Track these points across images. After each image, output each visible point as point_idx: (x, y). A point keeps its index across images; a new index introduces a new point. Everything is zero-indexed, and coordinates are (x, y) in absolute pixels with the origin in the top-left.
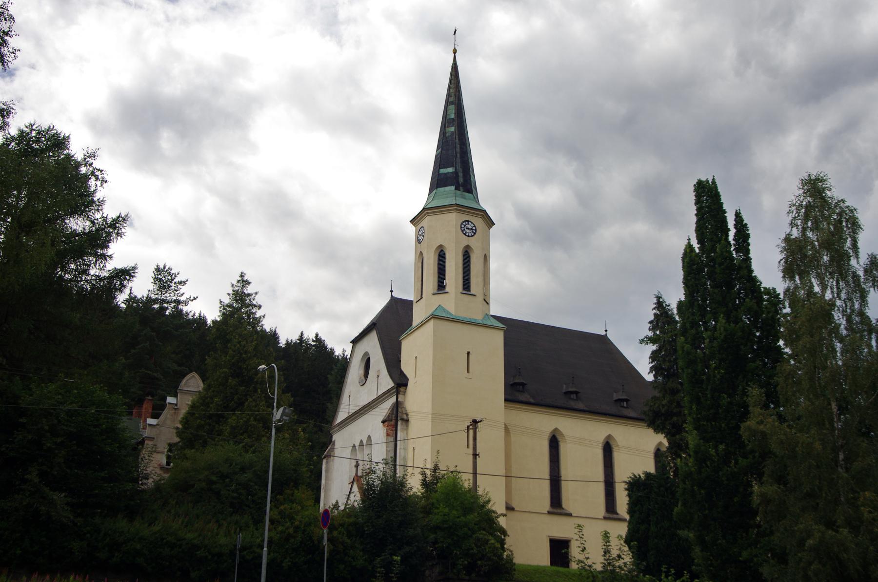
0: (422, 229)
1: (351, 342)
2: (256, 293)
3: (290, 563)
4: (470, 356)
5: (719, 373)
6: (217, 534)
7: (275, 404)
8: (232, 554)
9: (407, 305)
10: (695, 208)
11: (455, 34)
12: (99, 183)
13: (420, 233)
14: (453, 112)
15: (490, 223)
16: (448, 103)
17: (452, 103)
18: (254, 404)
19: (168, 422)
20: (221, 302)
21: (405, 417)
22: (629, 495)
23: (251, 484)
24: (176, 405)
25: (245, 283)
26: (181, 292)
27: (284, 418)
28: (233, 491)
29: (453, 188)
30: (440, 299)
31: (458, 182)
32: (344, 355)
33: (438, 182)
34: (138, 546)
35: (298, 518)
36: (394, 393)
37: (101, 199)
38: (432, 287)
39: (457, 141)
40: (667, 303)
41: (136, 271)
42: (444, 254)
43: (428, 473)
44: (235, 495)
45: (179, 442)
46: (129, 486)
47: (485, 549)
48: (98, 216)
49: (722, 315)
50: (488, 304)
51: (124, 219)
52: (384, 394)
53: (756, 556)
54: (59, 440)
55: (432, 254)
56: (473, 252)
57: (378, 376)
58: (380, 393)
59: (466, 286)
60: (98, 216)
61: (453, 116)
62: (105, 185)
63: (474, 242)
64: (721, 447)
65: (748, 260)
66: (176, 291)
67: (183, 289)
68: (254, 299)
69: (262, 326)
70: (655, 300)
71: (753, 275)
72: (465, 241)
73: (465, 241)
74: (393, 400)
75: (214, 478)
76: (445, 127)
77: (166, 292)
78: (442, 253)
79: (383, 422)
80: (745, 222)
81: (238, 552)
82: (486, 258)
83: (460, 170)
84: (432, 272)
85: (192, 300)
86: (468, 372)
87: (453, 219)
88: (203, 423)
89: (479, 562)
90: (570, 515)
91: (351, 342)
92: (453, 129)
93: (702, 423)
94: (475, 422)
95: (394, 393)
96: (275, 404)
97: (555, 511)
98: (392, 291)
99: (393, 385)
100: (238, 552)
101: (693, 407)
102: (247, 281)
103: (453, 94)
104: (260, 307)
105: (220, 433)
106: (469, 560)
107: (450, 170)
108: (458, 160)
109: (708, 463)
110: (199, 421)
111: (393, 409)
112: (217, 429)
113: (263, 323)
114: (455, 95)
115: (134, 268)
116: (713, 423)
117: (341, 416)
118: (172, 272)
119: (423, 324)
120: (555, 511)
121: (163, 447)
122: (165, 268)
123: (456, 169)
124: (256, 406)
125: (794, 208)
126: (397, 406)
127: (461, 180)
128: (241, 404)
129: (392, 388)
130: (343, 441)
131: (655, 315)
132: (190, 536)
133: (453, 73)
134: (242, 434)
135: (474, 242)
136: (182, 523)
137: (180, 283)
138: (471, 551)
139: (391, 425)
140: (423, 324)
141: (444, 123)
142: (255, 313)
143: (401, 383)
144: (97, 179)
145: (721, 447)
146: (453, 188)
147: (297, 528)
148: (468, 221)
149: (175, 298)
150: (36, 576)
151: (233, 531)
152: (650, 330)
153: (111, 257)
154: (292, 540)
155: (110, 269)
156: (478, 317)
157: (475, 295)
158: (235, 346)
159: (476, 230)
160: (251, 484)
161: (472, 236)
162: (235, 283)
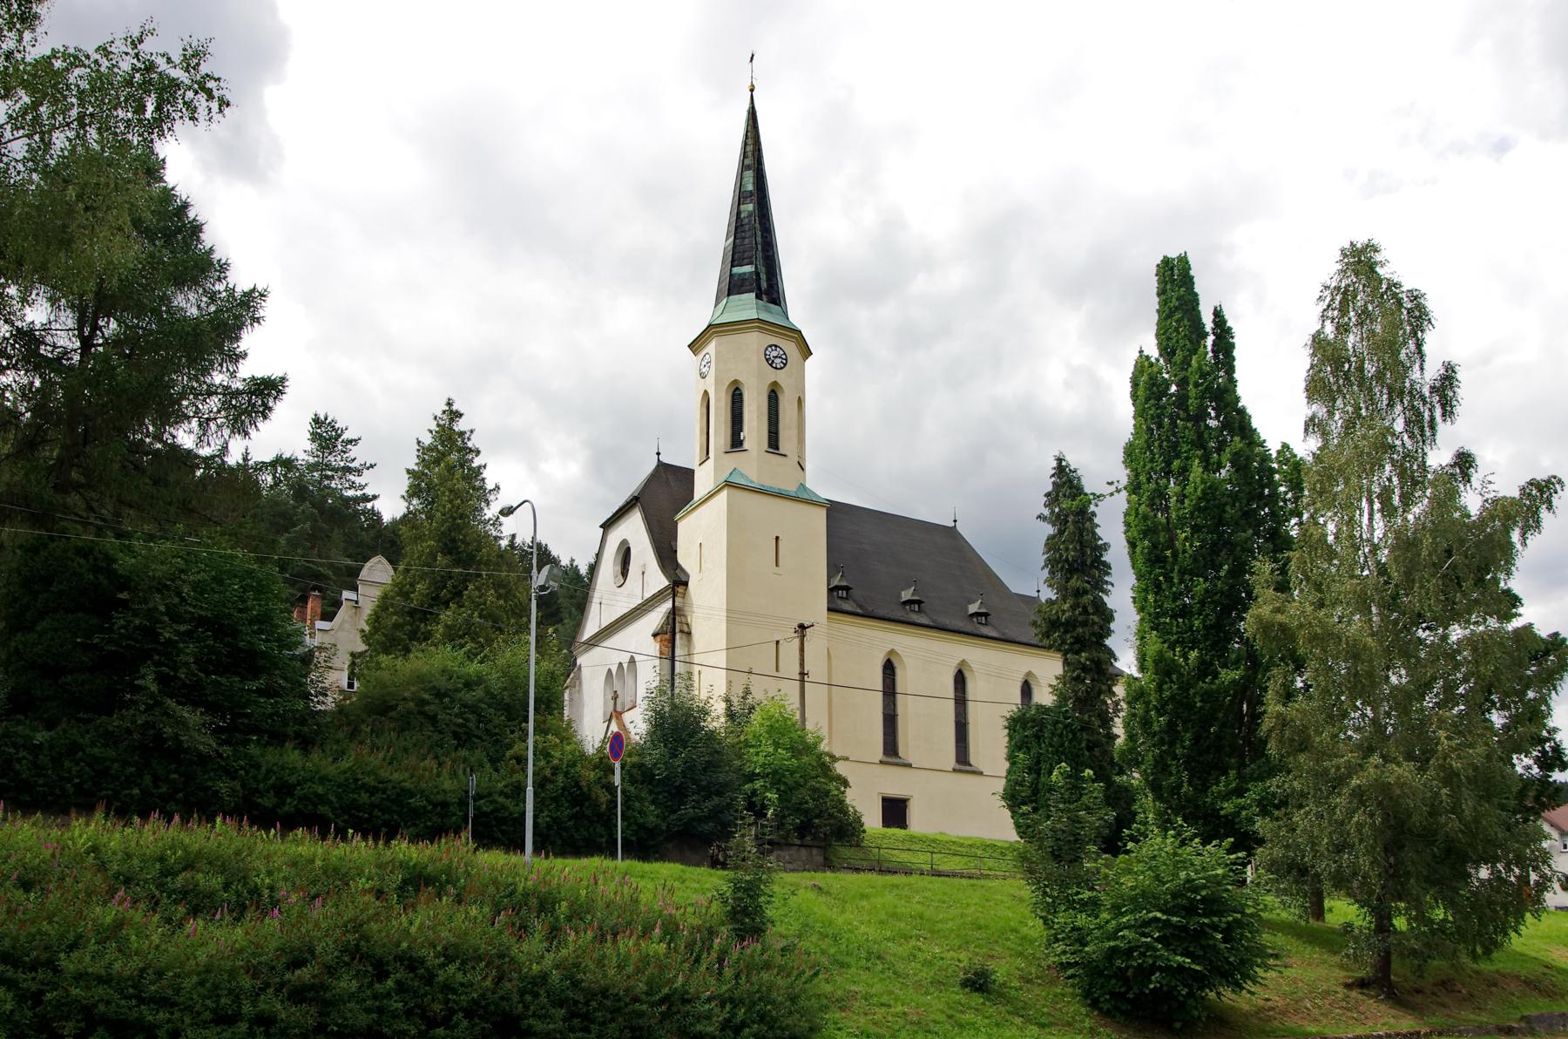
0: (707, 356)
1: (601, 526)
2: (472, 431)
3: (548, 819)
4: (780, 542)
5: (1191, 546)
6: (438, 775)
7: (534, 562)
8: (463, 803)
9: (686, 476)
10: (1157, 299)
11: (751, 60)
12: (215, 105)
13: (704, 363)
14: (751, 180)
15: (806, 352)
16: (743, 167)
17: (748, 168)
18: (477, 593)
19: (347, 626)
20: (419, 442)
21: (686, 629)
22: (1009, 735)
23: (483, 706)
24: (357, 602)
25: (455, 415)
26: (352, 455)
27: (551, 583)
28: (456, 715)
29: (753, 295)
30: (735, 459)
31: (759, 288)
32: (572, 565)
33: (733, 286)
34: (320, 790)
35: (557, 754)
36: (668, 594)
37: (223, 261)
38: (723, 442)
39: (757, 225)
40: (1072, 468)
41: (287, 384)
42: (741, 395)
43: (735, 701)
44: (461, 721)
45: (366, 651)
46: (300, 705)
47: (826, 803)
48: (220, 287)
49: (1197, 461)
50: (803, 469)
51: (262, 295)
52: (654, 597)
53: (1243, 808)
54: (183, 628)
55: (723, 394)
56: (783, 392)
57: (643, 573)
58: (648, 595)
59: (774, 443)
60: (220, 287)
61: (750, 187)
62: (227, 111)
63: (781, 377)
64: (1194, 654)
65: (1232, 382)
66: (345, 452)
67: (354, 451)
68: (469, 439)
69: (483, 479)
70: (1054, 464)
71: (1240, 405)
72: (772, 375)
73: (772, 375)
74: (668, 605)
75: (426, 696)
76: (739, 204)
77: (330, 454)
78: (738, 392)
79: (655, 635)
80: (1228, 324)
81: (471, 801)
82: (800, 402)
83: (762, 270)
84: (723, 419)
85: (368, 469)
86: (777, 565)
87: (755, 342)
88: (401, 621)
89: (817, 821)
90: (910, 766)
91: (601, 526)
92: (750, 207)
93: (1162, 620)
94: (802, 627)
95: (668, 594)
96: (534, 562)
97: (889, 760)
98: (658, 454)
99: (667, 583)
100: (471, 801)
101: (1149, 597)
102: (457, 411)
103: (750, 154)
104: (478, 452)
105: (427, 636)
106: (802, 818)
107: (748, 269)
108: (760, 254)
109: (1174, 677)
110: (395, 617)
111: (668, 617)
112: (423, 630)
113: (483, 476)
114: (753, 155)
115: (283, 379)
116: (1180, 620)
117: (590, 628)
118: (337, 426)
119: (711, 496)
120: (889, 760)
121: (342, 661)
122: (326, 419)
123: (756, 268)
124: (480, 597)
125: (1327, 293)
126: (674, 613)
127: (764, 285)
128: (457, 594)
129: (666, 589)
130: (593, 666)
131: (1054, 483)
132: (396, 776)
133: (751, 122)
134: (461, 637)
135: (781, 377)
136: (384, 760)
137: (350, 442)
138: (806, 806)
139: (666, 640)
140: (711, 496)
141: (737, 198)
142: (472, 461)
143: (678, 581)
144: (210, 96)
145: (1194, 654)
146: (753, 295)
147: (555, 770)
148: (776, 346)
149: (342, 464)
150: (157, 816)
151: (461, 772)
152: (1045, 506)
153: (244, 355)
154: (549, 786)
155: (246, 377)
156: (791, 488)
157: (785, 456)
158: (444, 507)
159: (786, 360)
160: (483, 706)
161: (781, 368)
162: (439, 414)
